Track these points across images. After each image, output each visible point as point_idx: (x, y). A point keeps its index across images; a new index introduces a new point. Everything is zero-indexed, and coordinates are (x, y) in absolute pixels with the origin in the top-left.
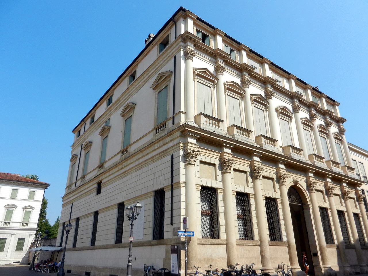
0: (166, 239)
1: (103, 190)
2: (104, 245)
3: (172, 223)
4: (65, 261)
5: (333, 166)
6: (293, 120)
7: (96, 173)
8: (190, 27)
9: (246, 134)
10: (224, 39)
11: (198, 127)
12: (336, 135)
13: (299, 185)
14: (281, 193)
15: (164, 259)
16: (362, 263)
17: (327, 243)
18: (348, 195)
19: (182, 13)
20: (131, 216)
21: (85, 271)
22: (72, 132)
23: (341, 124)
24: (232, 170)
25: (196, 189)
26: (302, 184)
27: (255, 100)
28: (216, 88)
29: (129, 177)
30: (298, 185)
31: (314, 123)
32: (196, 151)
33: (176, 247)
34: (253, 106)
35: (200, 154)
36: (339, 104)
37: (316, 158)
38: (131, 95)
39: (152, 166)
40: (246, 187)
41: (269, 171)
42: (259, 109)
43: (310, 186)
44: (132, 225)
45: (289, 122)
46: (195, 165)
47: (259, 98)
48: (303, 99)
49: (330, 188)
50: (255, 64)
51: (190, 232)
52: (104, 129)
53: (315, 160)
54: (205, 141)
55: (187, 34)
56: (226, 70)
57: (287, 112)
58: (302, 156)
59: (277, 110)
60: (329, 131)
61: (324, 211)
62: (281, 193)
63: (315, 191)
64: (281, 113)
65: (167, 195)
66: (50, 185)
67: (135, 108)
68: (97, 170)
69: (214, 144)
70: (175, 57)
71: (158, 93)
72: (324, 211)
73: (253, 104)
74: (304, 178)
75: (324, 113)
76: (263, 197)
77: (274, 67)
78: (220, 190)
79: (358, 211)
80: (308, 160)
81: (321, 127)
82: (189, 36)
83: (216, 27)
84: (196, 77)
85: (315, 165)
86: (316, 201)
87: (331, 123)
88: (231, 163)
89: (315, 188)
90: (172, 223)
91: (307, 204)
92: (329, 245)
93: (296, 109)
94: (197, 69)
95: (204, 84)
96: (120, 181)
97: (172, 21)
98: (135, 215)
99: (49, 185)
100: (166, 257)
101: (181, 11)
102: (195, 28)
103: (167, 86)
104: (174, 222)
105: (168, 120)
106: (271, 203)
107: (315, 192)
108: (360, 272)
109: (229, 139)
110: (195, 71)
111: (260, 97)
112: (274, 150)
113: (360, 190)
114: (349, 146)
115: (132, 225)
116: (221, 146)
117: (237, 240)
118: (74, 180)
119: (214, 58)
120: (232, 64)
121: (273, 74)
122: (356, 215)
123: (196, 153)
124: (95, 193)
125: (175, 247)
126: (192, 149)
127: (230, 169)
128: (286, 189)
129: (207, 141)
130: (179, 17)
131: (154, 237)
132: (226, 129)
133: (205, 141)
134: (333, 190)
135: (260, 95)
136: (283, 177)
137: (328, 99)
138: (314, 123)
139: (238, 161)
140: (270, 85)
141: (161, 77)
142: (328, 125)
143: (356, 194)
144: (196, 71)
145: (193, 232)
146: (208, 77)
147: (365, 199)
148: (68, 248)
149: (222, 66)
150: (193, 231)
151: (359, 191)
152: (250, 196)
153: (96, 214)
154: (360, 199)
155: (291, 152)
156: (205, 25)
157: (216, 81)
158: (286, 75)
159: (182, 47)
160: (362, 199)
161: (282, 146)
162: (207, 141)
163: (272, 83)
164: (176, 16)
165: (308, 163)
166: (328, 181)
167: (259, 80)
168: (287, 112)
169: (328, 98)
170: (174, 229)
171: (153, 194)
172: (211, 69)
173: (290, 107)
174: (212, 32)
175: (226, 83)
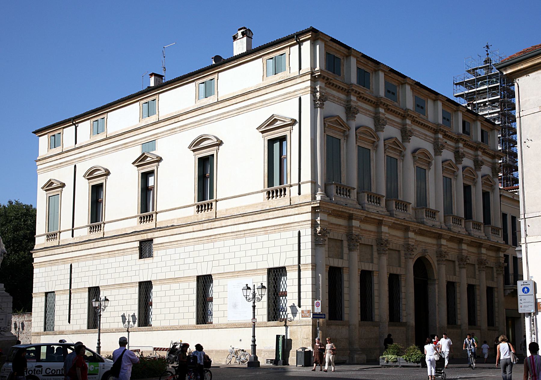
44: (254, 307)
45: (427, 171)
115: (254, 307)
122: (490, 290)
124: (137, 255)
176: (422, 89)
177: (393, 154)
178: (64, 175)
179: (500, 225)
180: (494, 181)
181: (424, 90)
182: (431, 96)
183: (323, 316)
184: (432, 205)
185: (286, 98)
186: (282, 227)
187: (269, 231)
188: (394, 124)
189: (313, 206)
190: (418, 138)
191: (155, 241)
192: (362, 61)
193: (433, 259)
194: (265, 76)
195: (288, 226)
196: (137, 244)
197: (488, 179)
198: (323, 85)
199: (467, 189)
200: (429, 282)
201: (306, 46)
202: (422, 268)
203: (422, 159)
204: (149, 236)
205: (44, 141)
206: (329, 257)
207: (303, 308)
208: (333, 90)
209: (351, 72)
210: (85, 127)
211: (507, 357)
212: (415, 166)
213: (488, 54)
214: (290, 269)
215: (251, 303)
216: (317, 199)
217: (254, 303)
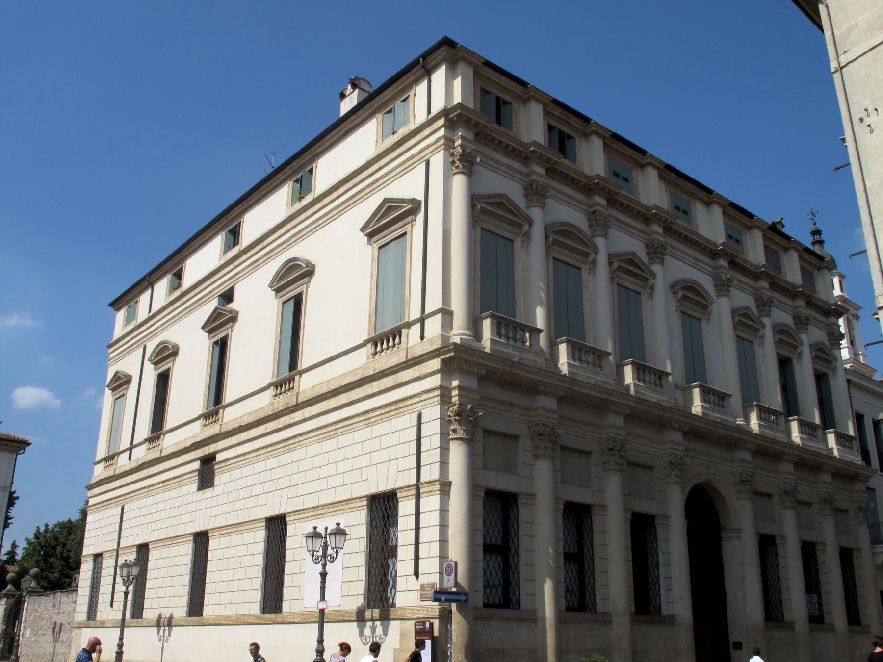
0: (401, 608)
1: (218, 479)
2: (230, 616)
4: (124, 649)
7: (196, 432)
15: (395, 650)
20: (320, 553)
22: (111, 305)
29: (298, 454)
33: (427, 625)
38: (300, 236)
39: (363, 434)
42: (629, 292)
44: (324, 575)
47: (500, 205)
52: (216, 315)
65: (405, 507)
66: (30, 444)
68: (199, 423)
71: (380, 248)
77: (673, 175)
95: (566, 263)
96: (272, 463)
98: (330, 551)
99: (30, 444)
100: (401, 645)
101: (444, 48)
103: (405, 233)
105: (408, 325)
115: (324, 575)
118: (125, 443)
120: (567, 176)
124: (195, 486)
125: (424, 623)
140: (660, 225)
141: (390, 209)
146: (508, 216)
148: (148, 617)
153: (201, 540)
156: (503, 78)
158: (702, 194)
164: (432, 57)
170: (422, 586)
174: (520, 93)
176: (681, 179)
177: (629, 282)
178: (129, 364)
181: (686, 182)
182: (699, 195)
183: (463, 598)
185: (406, 168)
186: (393, 408)
187: (372, 420)
188: (631, 230)
189: (443, 357)
190: (681, 263)
191: (220, 457)
192: (557, 114)
193: (726, 488)
194: (380, 141)
195: (402, 405)
196: (196, 465)
197: (820, 350)
198: (471, 136)
199: (785, 365)
200: (724, 535)
201: (439, 76)
203: (691, 300)
204: (211, 448)
205: (121, 315)
206: (485, 468)
207: (423, 579)
208: (497, 151)
209: (532, 126)
210: (162, 286)
213: (815, 224)
214: (404, 494)
215: (319, 568)
217: (324, 566)
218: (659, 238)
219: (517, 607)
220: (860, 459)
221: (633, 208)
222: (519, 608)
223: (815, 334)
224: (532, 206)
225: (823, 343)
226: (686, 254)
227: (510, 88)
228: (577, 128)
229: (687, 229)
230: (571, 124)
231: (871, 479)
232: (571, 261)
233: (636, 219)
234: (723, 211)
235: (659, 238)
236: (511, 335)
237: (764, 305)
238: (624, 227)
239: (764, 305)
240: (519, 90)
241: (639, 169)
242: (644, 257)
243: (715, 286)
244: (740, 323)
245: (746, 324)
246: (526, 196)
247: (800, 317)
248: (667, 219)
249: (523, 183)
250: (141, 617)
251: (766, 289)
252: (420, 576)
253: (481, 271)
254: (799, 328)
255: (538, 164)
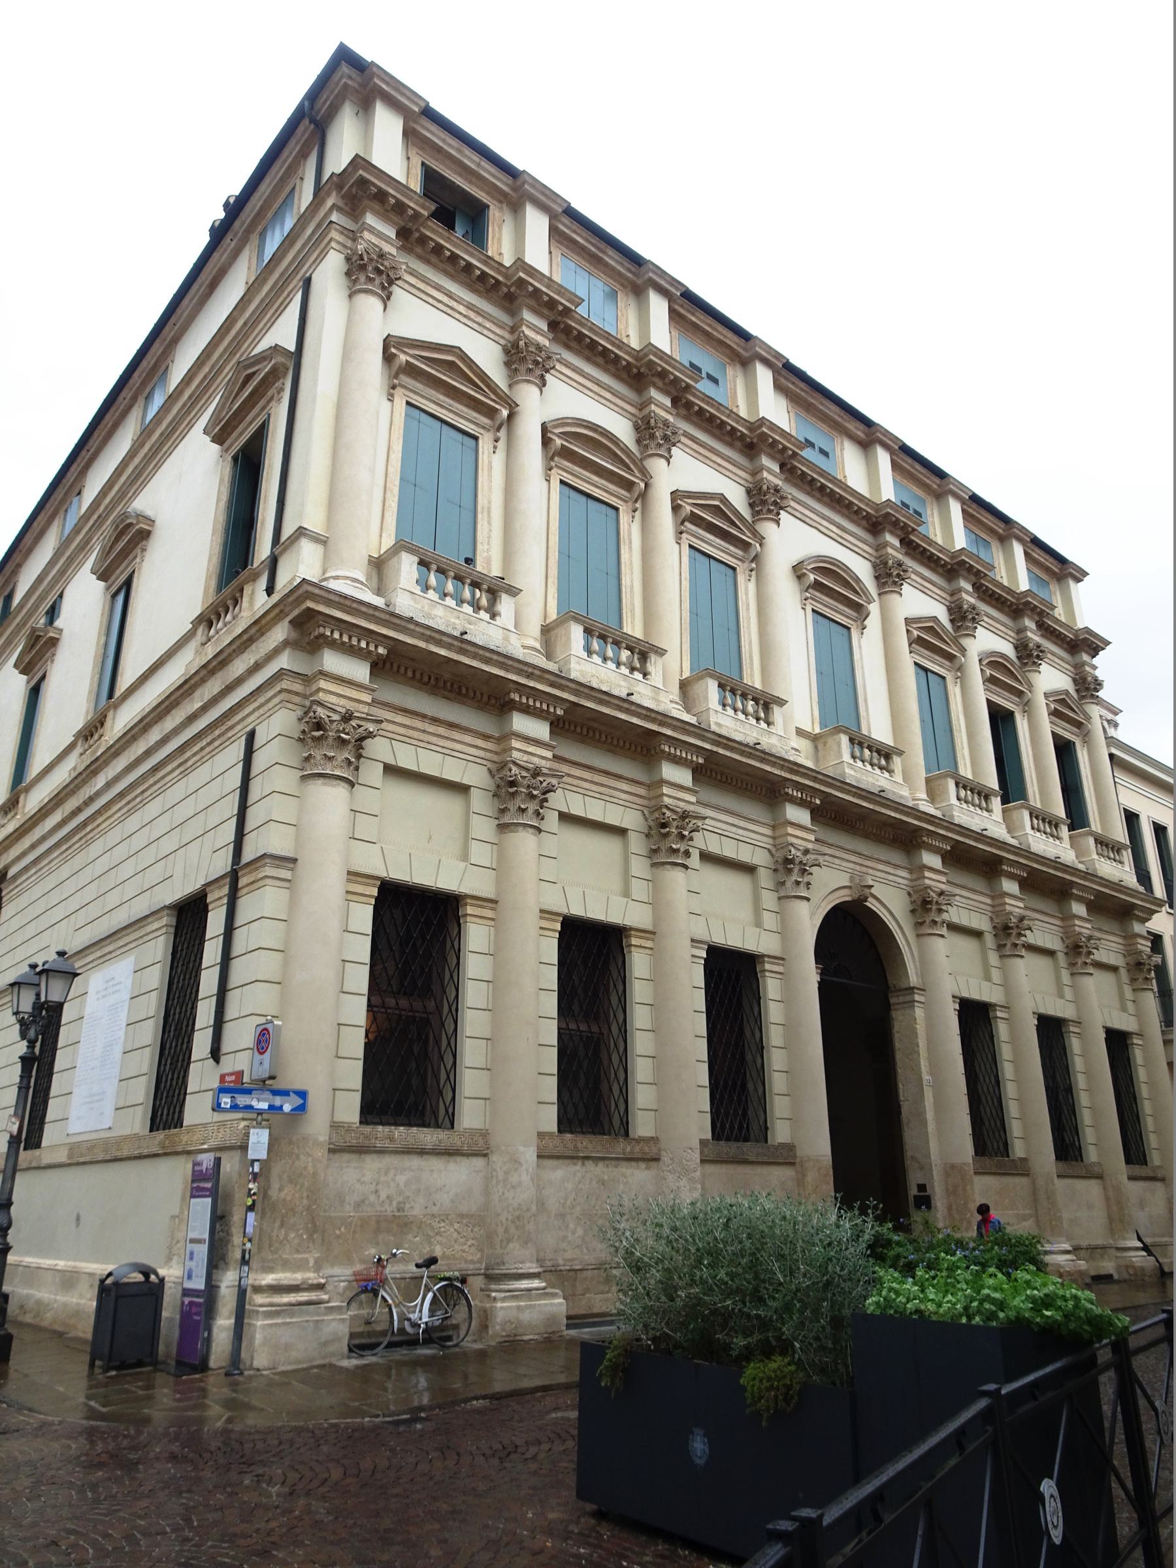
3: (216, 1054)
5: (1033, 828)
6: (874, 621)
8: (387, 149)
9: (756, 712)
10: (677, 307)
11: (383, 606)
12: (1062, 702)
13: (874, 902)
14: (785, 932)
16: (1124, 1239)
17: (1066, 1159)
18: (1090, 953)
19: (350, 78)
21: (101, 1268)
23: (1085, 657)
24: (695, 854)
25: (689, 958)
26: (890, 900)
27: (695, 519)
28: (638, 514)
30: (871, 904)
31: (967, 642)
32: (359, 718)
34: (555, 484)
35: (381, 732)
36: (1085, 574)
37: (1035, 821)
40: (752, 931)
41: (732, 829)
43: (924, 907)
45: (855, 634)
46: (686, 867)
47: (717, 511)
48: (1057, 621)
49: (1014, 920)
50: (706, 361)
51: (285, 1093)
53: (954, 801)
54: (603, 737)
55: (361, 172)
56: (558, 366)
57: (847, 584)
58: (898, 777)
59: (798, 571)
60: (1030, 686)
61: (975, 1018)
62: (785, 932)
63: (944, 931)
64: (818, 585)
67: (152, 536)
69: (464, 691)
70: (307, 283)
72: (975, 1018)
73: (684, 535)
74: (902, 876)
75: (1014, 607)
76: (541, 918)
78: (773, 963)
79: (1124, 1022)
80: (924, 796)
81: (993, 664)
82: (532, 285)
83: (519, 163)
84: (405, 379)
85: (952, 816)
86: (944, 970)
87: (1042, 651)
88: (545, 784)
89: (945, 916)
90: (216, 1054)
91: (904, 986)
92: (986, 1160)
93: (890, 575)
94: (689, 497)
95: (588, 496)
97: (306, 121)
102: (417, 161)
104: (226, 1047)
106: (732, 977)
107: (942, 936)
108: (1116, 1277)
109: (537, 672)
110: (393, 350)
111: (720, 506)
112: (988, 826)
113: (1145, 934)
114: (1114, 751)
116: (503, 706)
117: (703, 1143)
119: (630, 386)
121: (557, 254)
122: (1118, 1042)
123: (360, 726)
126: (342, 705)
127: (687, 854)
128: (807, 921)
129: (430, 678)
130: (336, 97)
131: (153, 1119)
132: (536, 631)
133: (603, 737)
134: (1028, 932)
135: (723, 498)
136: (801, 862)
137: (974, 506)
138: (967, 642)
139: (586, 780)
142: (1028, 655)
143: (1130, 951)
144: (405, 353)
145: (302, 1094)
147: (1161, 971)
149: (539, 348)
150: (298, 1086)
151: (1140, 941)
152: (767, 966)
154: (1147, 968)
155: (847, 757)
157: (642, 485)
159: (334, 234)
160: (1150, 970)
161: (808, 728)
162: (430, 678)
163: (902, 528)
165: (922, 808)
166: (930, 865)
167: (474, 277)
168: (847, 584)
169: (1037, 542)
171: (167, 920)
172: (737, 497)
173: (862, 569)
175: (556, 427)
179: (1120, 834)
180: (1085, 713)
184: (879, 729)
199: (1001, 720)
202: (855, 950)
207: (229, 1064)
211: (500, 1317)
212: (809, 608)
216: (1108, 1350)
218: (770, 478)
219: (449, 1125)
220: (1135, 880)
221: (723, 422)
222: (453, 1127)
223: (1051, 678)
224: (518, 382)
225: (1067, 692)
226: (824, 517)
227: (728, 341)
228: (620, 274)
229: (823, 473)
230: (607, 265)
231: (1155, 916)
232: (597, 493)
233: (730, 445)
234: (892, 461)
235: (770, 478)
236: (739, 705)
237: (962, 618)
238: (703, 454)
239: (962, 618)
240: (1000, 528)
241: (738, 367)
242: (496, 372)
243: (876, 577)
244: (920, 641)
245: (934, 644)
246: (507, 364)
247: (1027, 645)
248: (785, 448)
249: (503, 342)
250: (179, 1123)
251: (967, 592)
252: (223, 1058)
253: (403, 479)
254: (1084, 697)
255: (892, 533)
